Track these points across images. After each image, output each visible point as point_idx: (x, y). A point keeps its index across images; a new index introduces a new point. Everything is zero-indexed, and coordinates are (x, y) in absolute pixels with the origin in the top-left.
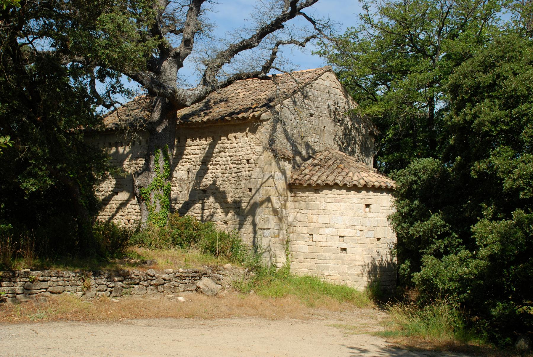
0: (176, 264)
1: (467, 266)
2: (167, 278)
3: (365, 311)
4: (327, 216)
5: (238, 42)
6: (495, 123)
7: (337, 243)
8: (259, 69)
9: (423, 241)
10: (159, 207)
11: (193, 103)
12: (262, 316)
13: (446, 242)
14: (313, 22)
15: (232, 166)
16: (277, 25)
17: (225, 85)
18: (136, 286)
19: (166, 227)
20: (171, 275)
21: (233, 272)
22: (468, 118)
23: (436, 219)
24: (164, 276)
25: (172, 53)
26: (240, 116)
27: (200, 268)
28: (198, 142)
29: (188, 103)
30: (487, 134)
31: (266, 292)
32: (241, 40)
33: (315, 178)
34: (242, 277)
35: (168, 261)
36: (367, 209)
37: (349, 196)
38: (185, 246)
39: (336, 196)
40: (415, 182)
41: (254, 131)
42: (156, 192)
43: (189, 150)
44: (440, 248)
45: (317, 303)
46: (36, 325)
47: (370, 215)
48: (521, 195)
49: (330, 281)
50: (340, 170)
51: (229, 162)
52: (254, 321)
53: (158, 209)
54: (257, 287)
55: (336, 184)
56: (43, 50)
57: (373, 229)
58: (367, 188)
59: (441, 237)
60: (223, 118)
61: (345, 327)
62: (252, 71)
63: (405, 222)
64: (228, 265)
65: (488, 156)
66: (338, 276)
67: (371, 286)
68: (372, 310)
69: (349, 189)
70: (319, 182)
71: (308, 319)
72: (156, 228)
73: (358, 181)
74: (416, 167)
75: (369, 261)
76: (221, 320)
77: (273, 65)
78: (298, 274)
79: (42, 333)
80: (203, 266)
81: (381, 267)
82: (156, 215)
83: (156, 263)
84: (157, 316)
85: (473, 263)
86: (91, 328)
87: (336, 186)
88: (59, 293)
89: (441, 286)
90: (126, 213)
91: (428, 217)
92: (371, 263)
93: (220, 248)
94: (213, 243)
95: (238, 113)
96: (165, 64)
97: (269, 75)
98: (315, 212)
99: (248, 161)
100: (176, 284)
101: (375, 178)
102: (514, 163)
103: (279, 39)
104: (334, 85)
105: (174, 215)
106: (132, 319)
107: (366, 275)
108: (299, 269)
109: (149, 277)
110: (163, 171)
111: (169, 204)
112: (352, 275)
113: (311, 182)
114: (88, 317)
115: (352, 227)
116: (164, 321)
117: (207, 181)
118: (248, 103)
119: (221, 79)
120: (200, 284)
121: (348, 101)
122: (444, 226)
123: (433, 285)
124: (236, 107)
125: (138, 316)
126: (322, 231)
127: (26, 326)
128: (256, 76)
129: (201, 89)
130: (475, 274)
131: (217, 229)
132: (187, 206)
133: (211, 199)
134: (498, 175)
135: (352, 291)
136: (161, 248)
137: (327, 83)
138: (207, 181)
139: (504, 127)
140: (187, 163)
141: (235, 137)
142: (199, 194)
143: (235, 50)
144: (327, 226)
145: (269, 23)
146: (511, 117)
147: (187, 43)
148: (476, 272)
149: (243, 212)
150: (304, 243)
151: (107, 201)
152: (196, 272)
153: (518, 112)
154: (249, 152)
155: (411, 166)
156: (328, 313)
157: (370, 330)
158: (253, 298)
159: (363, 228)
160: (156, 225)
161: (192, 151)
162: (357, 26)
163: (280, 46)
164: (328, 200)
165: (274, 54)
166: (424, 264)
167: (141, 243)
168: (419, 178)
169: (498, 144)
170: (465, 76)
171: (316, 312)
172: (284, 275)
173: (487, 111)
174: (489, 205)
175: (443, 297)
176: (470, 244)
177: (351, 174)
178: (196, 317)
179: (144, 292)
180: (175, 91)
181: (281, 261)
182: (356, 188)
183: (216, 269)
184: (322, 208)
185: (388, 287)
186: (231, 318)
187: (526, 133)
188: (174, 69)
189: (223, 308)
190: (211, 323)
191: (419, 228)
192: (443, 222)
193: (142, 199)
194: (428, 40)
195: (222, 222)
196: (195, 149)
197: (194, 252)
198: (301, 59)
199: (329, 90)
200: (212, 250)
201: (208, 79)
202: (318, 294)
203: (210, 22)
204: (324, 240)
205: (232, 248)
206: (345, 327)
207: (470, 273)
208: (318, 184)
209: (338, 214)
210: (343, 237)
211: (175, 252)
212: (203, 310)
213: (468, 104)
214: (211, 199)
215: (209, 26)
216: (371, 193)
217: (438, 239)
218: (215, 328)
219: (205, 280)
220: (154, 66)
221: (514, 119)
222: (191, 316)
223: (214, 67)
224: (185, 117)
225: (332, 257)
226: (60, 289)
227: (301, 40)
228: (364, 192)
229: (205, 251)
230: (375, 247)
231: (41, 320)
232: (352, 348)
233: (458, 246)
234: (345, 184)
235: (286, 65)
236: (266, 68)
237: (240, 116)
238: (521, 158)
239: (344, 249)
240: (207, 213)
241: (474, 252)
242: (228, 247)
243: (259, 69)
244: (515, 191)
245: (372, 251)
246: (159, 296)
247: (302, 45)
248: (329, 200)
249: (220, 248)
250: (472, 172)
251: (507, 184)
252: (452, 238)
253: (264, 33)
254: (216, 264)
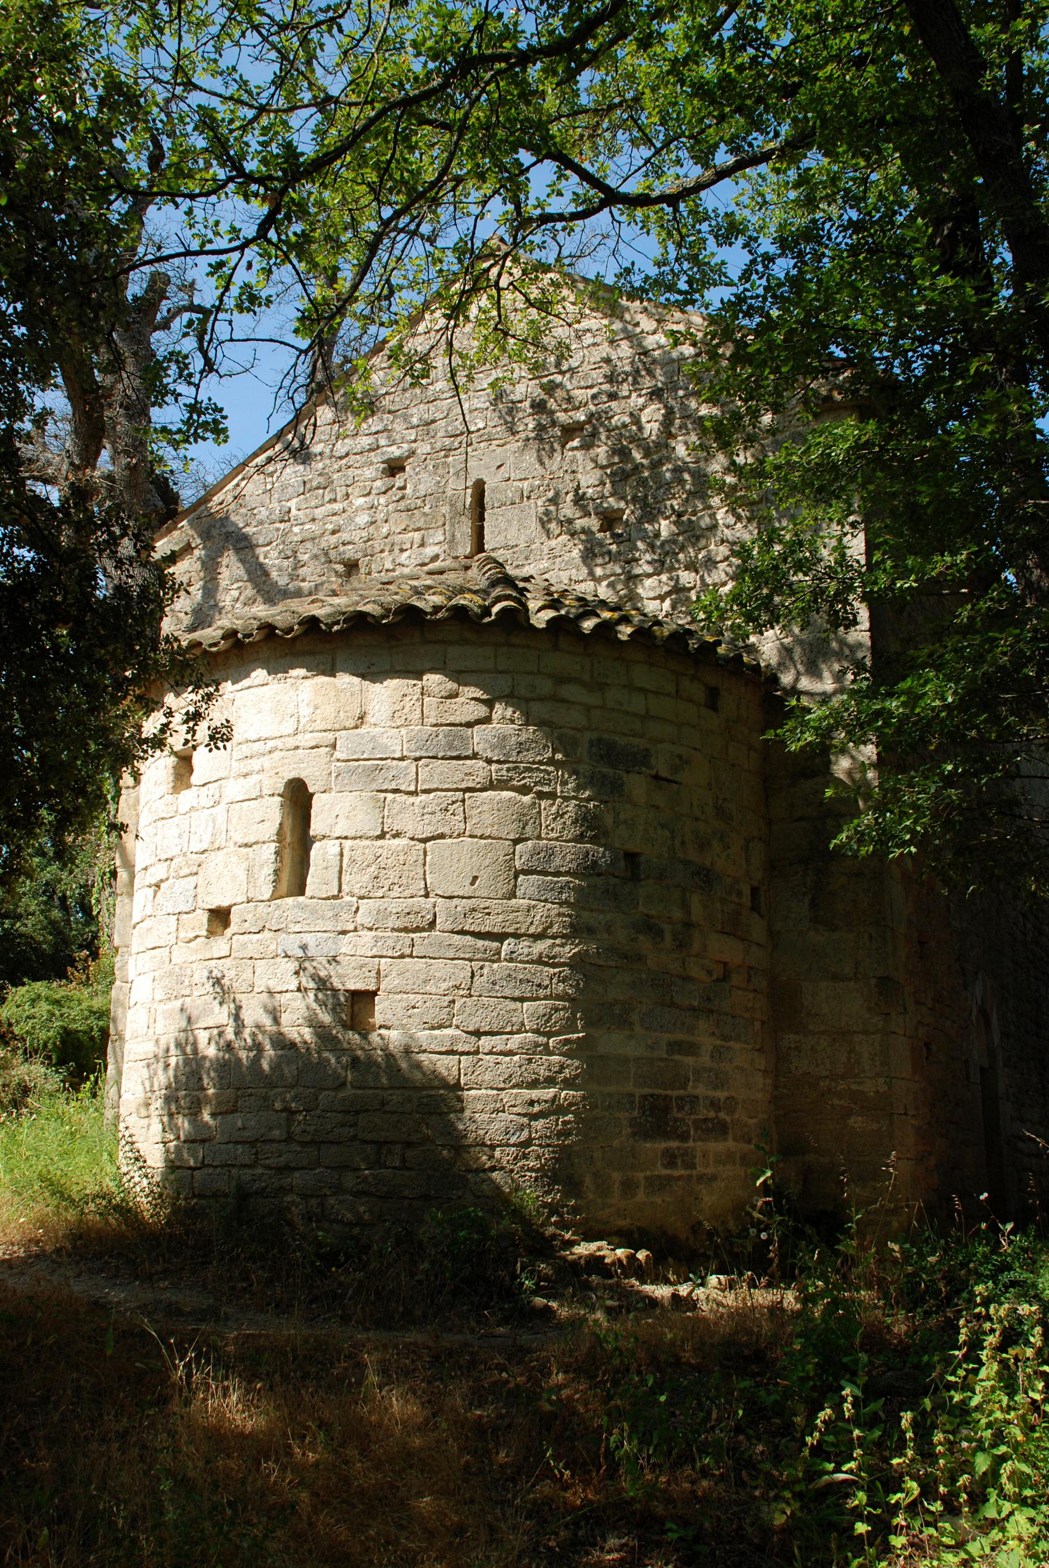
92: (178, 1045)
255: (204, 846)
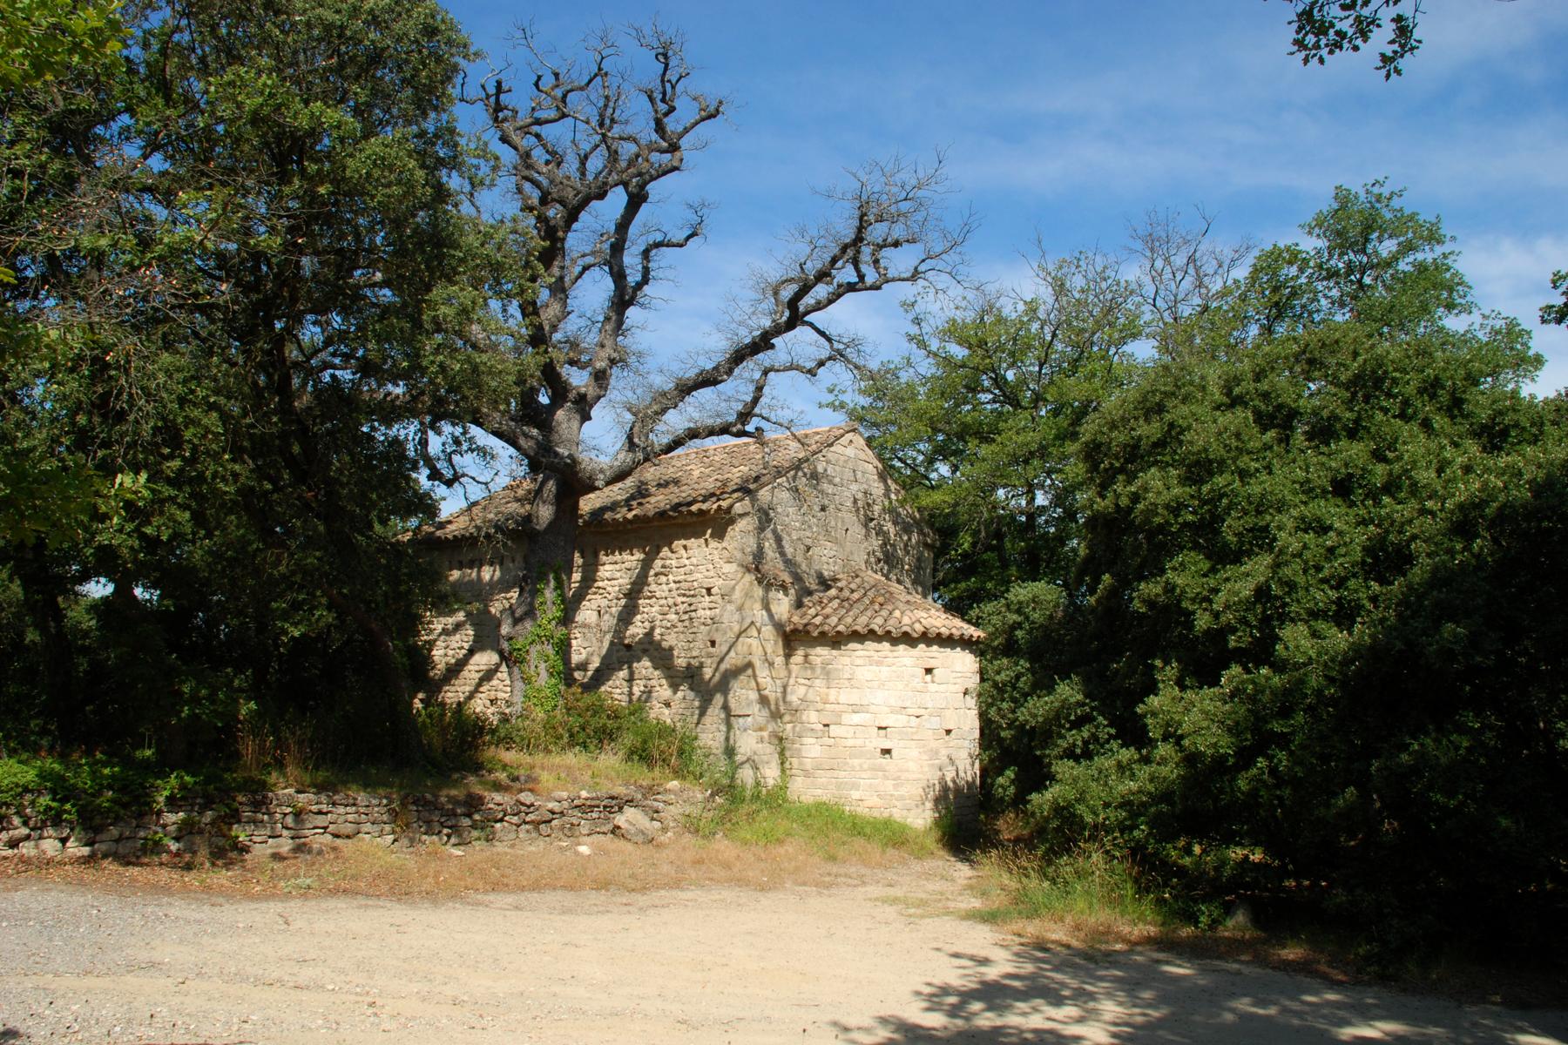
0: (575, 781)
1: (1133, 777)
2: (557, 809)
3: (929, 864)
5: (691, 374)
6: (1176, 508)
8: (732, 418)
9: (1045, 733)
10: (544, 674)
11: (608, 484)
12: (741, 882)
13: (1086, 735)
14: (829, 339)
15: (680, 599)
16: (763, 343)
17: (670, 448)
18: (498, 825)
19: (558, 712)
20: (565, 804)
21: (682, 797)
22: (1124, 502)
23: (1068, 691)
24: (550, 805)
25: (572, 396)
26: (694, 508)
27: (620, 790)
28: (617, 557)
29: (599, 483)
30: (1161, 529)
31: (745, 833)
32: (697, 371)
33: (833, 620)
34: (700, 806)
35: (563, 776)
36: (929, 677)
38: (592, 747)
40: (1019, 625)
41: (720, 535)
42: (539, 647)
43: (605, 571)
44: (1074, 745)
45: (841, 852)
46: (292, 904)
48: (1232, 642)
49: (862, 810)
50: (877, 607)
51: (674, 593)
52: (728, 894)
53: (543, 679)
54: (728, 825)
55: (872, 632)
57: (939, 713)
58: (928, 638)
59: (1078, 724)
60: (662, 514)
61: (906, 903)
62: (719, 421)
63: (1003, 700)
64: (674, 784)
65: (1163, 571)
66: (873, 801)
67: (937, 822)
68: (940, 863)
69: (895, 641)
70: (841, 628)
71: (829, 886)
72: (540, 714)
73: (911, 626)
74: (1021, 598)
75: (934, 778)
76: (663, 892)
77: (757, 410)
78: (803, 798)
79: (299, 923)
80: (626, 784)
81: (958, 790)
82: (539, 691)
83: (535, 780)
84: (536, 887)
85: (1144, 772)
86: (398, 913)
87: (872, 636)
88: (348, 837)
89: (1089, 819)
91: (1050, 689)
93: (656, 750)
94: (645, 742)
95: (690, 504)
96: (560, 414)
97: (750, 428)
99: (709, 590)
100: (575, 821)
101: (939, 620)
102: (1212, 583)
103: (767, 364)
104: (863, 456)
105: (574, 689)
106: (486, 892)
107: (929, 805)
108: (804, 791)
109: (522, 808)
110: (554, 612)
111: (566, 673)
112: (902, 798)
113: (826, 628)
114: (398, 889)
115: (901, 712)
116: (552, 897)
117: (637, 630)
118: (710, 485)
119: (660, 438)
120: (619, 820)
121: (888, 489)
122: (1080, 704)
123: (1074, 815)
124: (684, 493)
125: (497, 886)
126: (846, 718)
127: (272, 904)
128: (725, 430)
129: (625, 458)
130: (1150, 793)
131: (652, 716)
132: (601, 676)
133: (646, 663)
134: (1184, 605)
135: (903, 828)
136: (548, 751)
137: (850, 452)
138: (637, 630)
139: (1190, 517)
141: (685, 547)
142: (622, 654)
143: (686, 389)
144: (856, 709)
145: (747, 341)
146: (1200, 499)
147: (600, 377)
148: (1151, 787)
149: (705, 686)
150: (813, 741)
151: (455, 670)
152: (613, 798)
153: (1212, 490)
154: (712, 573)
155: (1011, 596)
156: (863, 871)
157: (951, 905)
158: (722, 846)
160: (538, 709)
162: (897, 360)
163: (771, 375)
164: (858, 657)
165: (759, 389)
166: (1059, 777)
167: (507, 741)
168: (1027, 618)
169: (1182, 548)
170: (1113, 426)
171: (842, 871)
172: (774, 800)
173: (1159, 487)
174: (1167, 662)
175: (1093, 838)
176: (1133, 733)
177: (897, 613)
178: (612, 888)
179: (513, 835)
180: (575, 462)
181: (771, 774)
182: (908, 639)
183: (650, 791)
185: (967, 824)
186: (682, 890)
187: (1229, 527)
188: (575, 424)
189: (665, 868)
190: (642, 900)
191: (1037, 709)
192: (1080, 697)
193: (511, 659)
194: (1022, 382)
195: (668, 705)
196: (616, 570)
197: (610, 760)
198: (804, 405)
199: (854, 464)
200: (642, 755)
201: (636, 440)
202: (845, 836)
203: (641, 348)
205: (681, 752)
206: (906, 903)
207: (1140, 791)
208: (838, 632)
211: (573, 758)
212: (627, 872)
213: (1121, 477)
214: (646, 663)
215: (640, 355)
216: (935, 647)
217: (1070, 729)
218: (652, 912)
219: (630, 812)
220: (539, 418)
221: (1205, 503)
222: (603, 885)
223: (645, 417)
224: (598, 513)
226: (349, 829)
227: (810, 365)
228: (922, 646)
229: (629, 758)
230: (944, 748)
231: (306, 893)
232: (956, 955)
233: (1108, 741)
234: (889, 632)
235: (779, 412)
236: (744, 416)
237: (694, 508)
238: (1222, 575)
239: (887, 752)
240: (636, 690)
241: (1144, 752)
242: (674, 748)
243: (732, 418)
244: (1218, 636)
245: (937, 753)
246: (541, 843)
247: (812, 372)
248: (858, 662)
249: (656, 750)
250: (1136, 601)
251: (1202, 621)
252: (1097, 727)
253: (740, 356)
254: (650, 782)
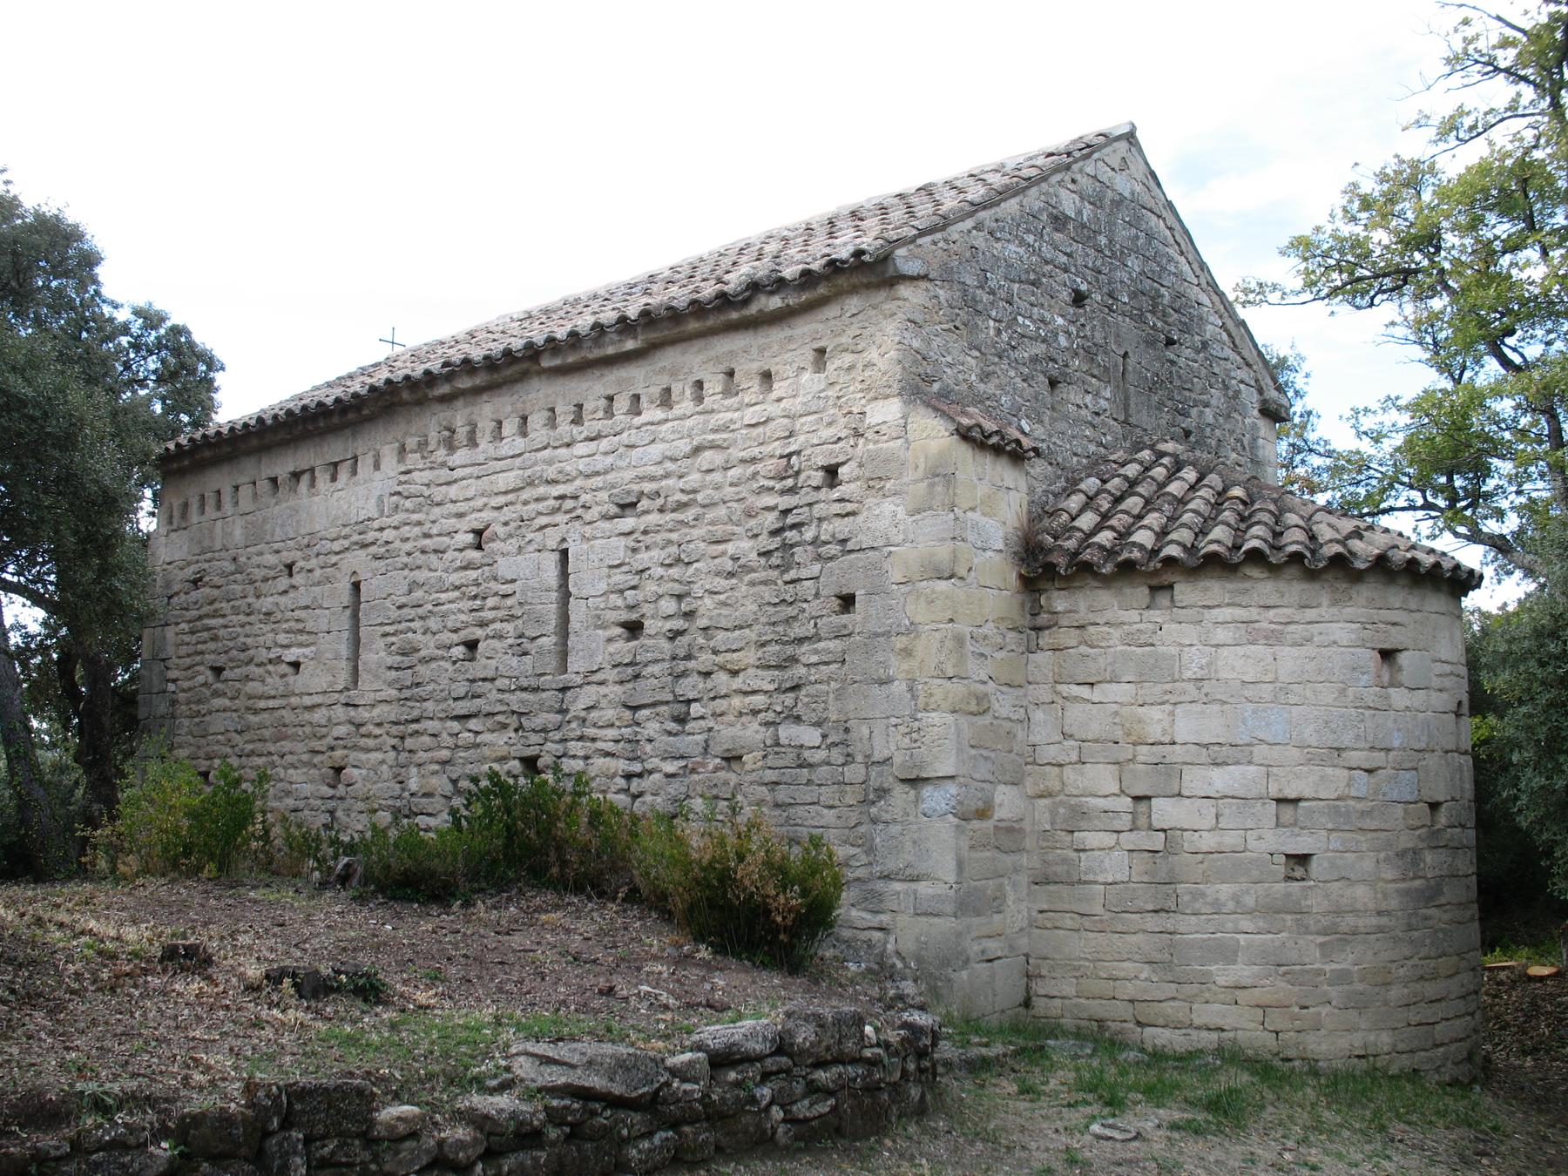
4: (1216, 707)
7: (1269, 835)
37: (1311, 614)
39: (1254, 613)
47: (1399, 697)
56: (530, 763)
90: (329, 740)
98: (1153, 691)
140: (560, 518)
150: (1109, 840)
159: (1378, 758)
161: (581, 465)
184: (1188, 674)
204: (1209, 822)
209: (1268, 697)
210: (1296, 801)
225: (1249, 901)
239: (1303, 859)
248: (1222, 635)
255: (1423, 745)
